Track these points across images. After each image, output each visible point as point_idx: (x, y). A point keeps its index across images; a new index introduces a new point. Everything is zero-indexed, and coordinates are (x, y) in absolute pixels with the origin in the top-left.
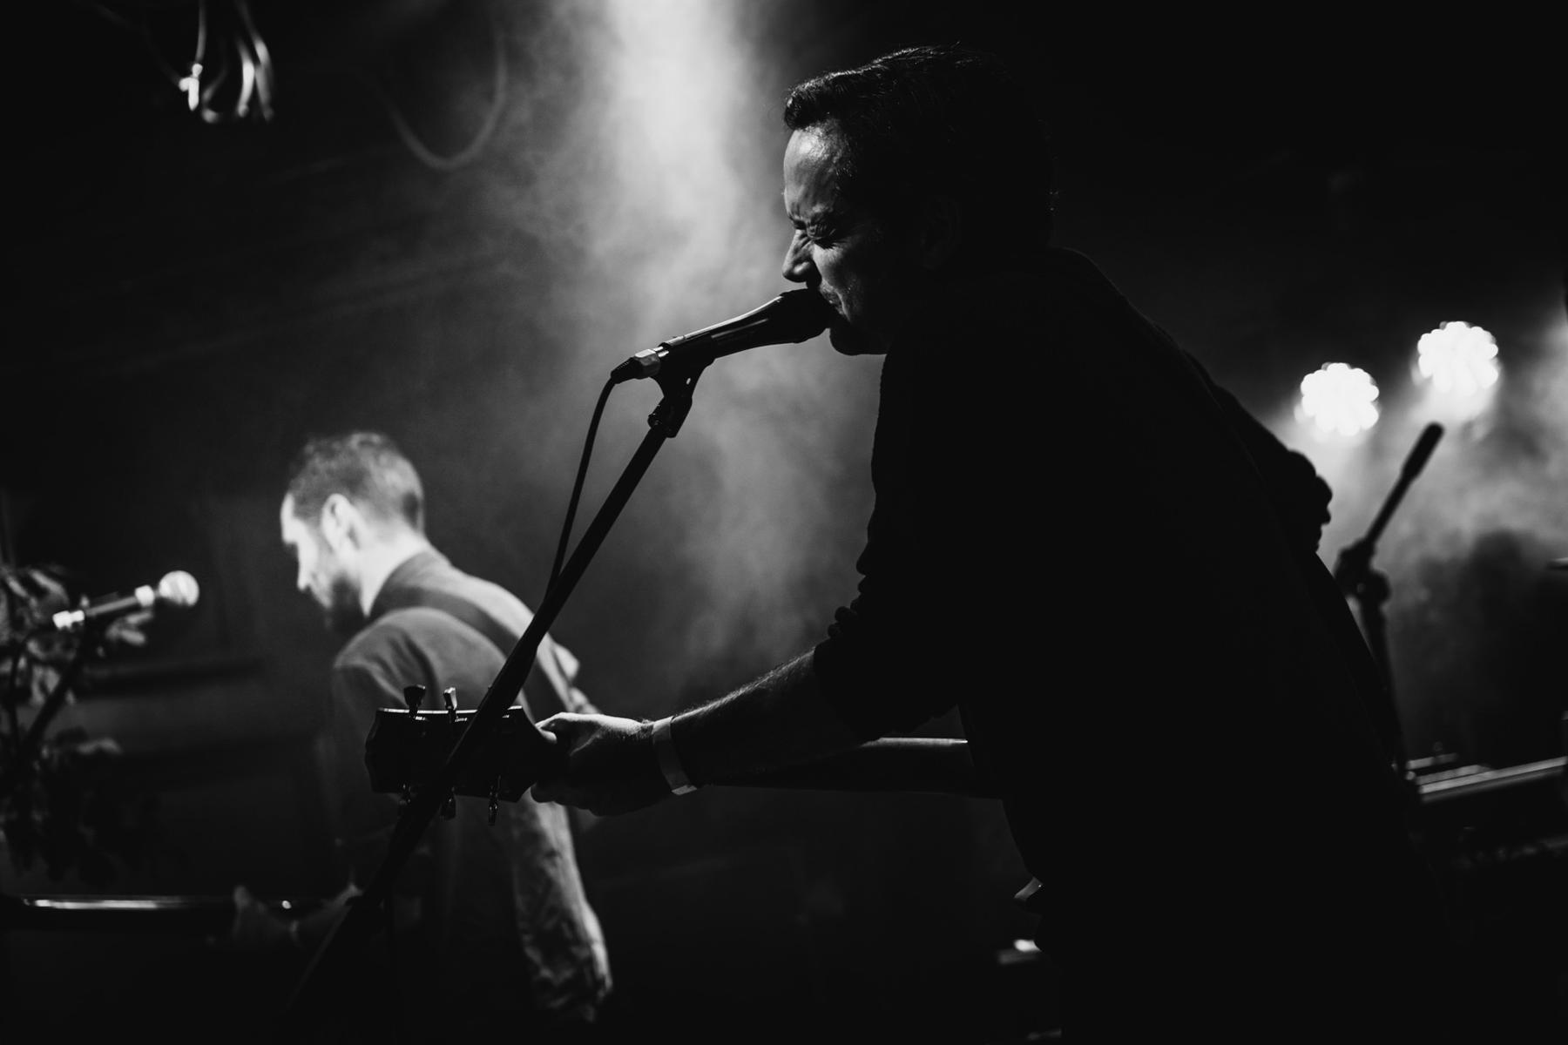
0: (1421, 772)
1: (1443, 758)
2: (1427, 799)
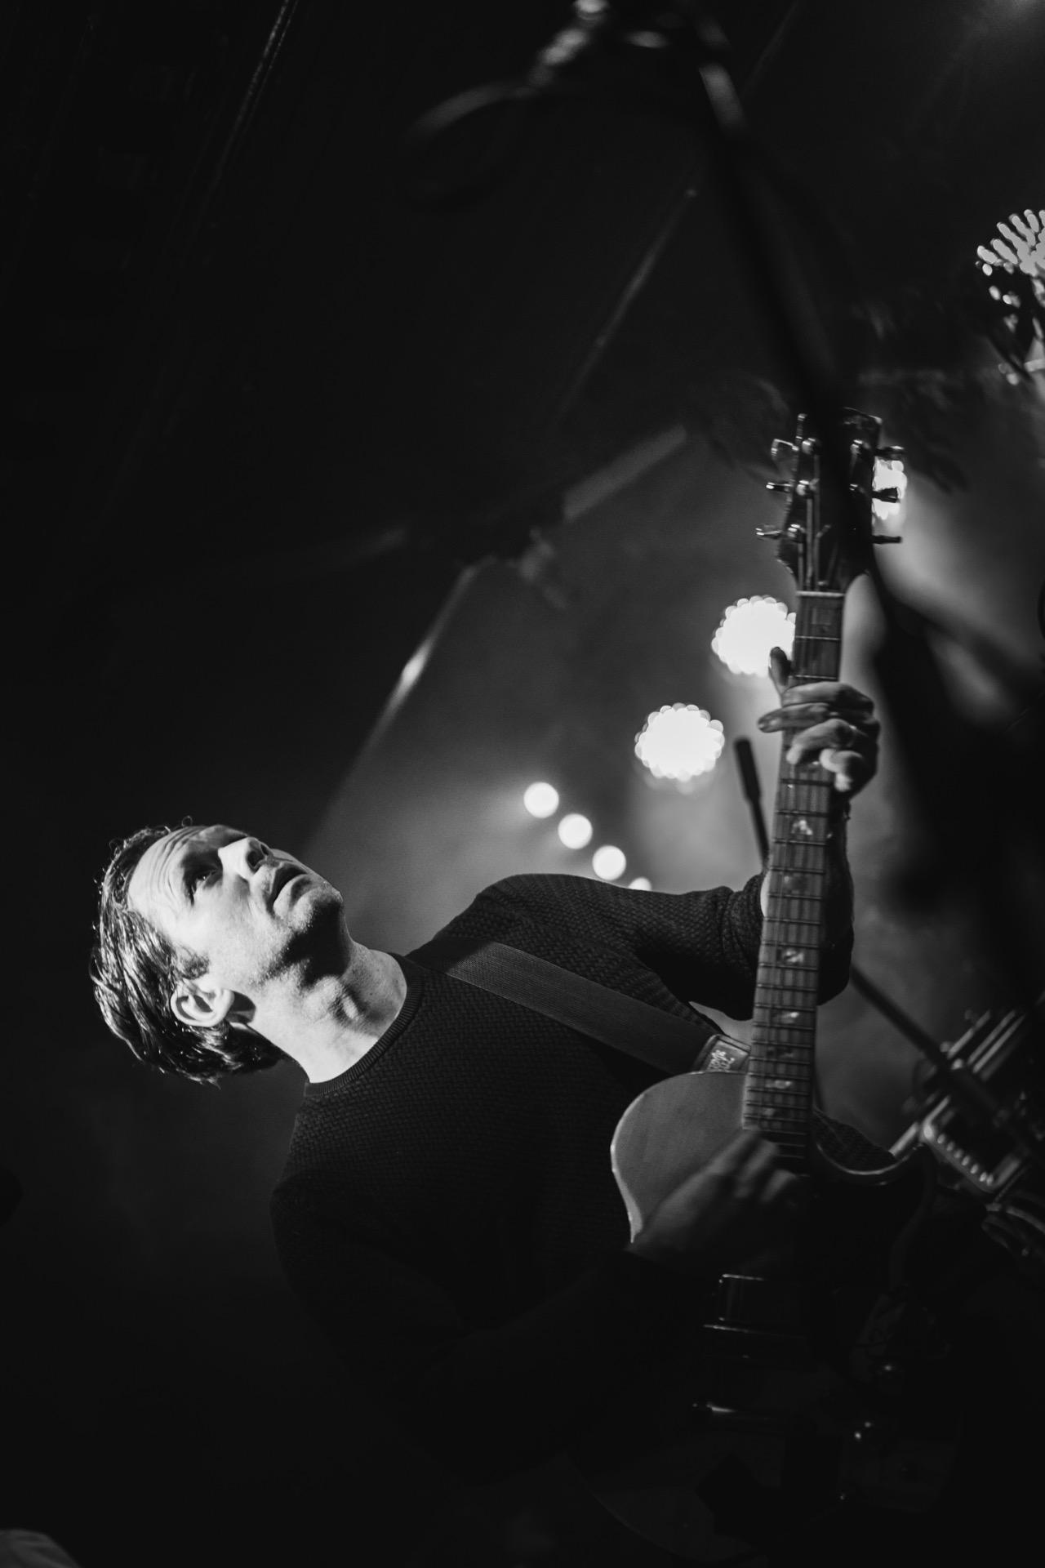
0: (964, 1054)
1: (980, 1023)
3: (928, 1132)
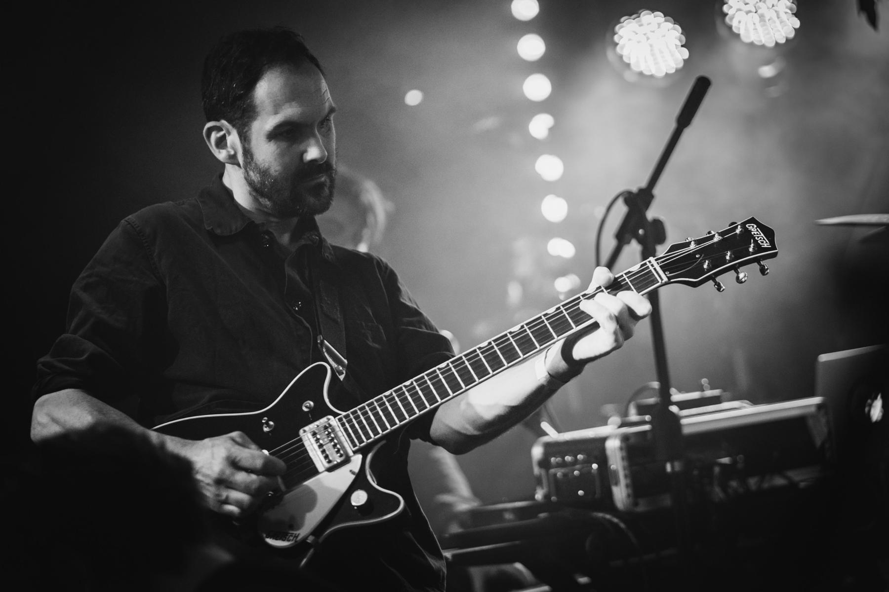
0: (683, 405)
2: (686, 431)
3: (611, 433)
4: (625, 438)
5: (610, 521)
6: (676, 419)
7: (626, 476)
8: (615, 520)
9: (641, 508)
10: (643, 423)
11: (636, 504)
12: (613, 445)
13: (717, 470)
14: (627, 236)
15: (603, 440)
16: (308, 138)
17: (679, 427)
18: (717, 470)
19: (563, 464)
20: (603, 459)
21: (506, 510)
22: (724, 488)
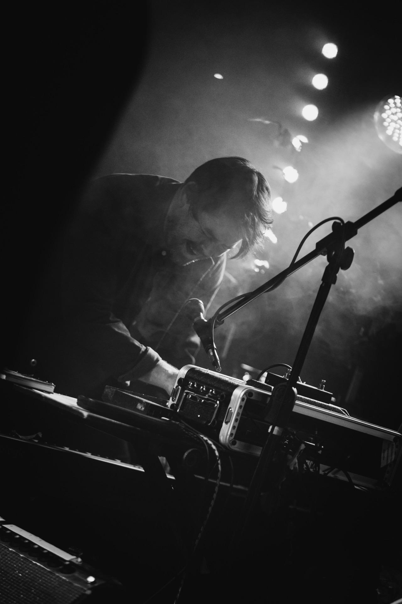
0: (299, 387)
2: (296, 409)
4: (249, 394)
5: (210, 446)
6: (293, 398)
7: (236, 420)
8: (214, 447)
9: (235, 448)
10: (269, 389)
11: (234, 443)
12: (238, 393)
13: (303, 447)
14: (325, 249)
15: (235, 387)
16: (367, 321)
17: (293, 404)
18: (303, 447)
19: (197, 390)
20: (226, 400)
21: (141, 402)
22: (301, 462)
